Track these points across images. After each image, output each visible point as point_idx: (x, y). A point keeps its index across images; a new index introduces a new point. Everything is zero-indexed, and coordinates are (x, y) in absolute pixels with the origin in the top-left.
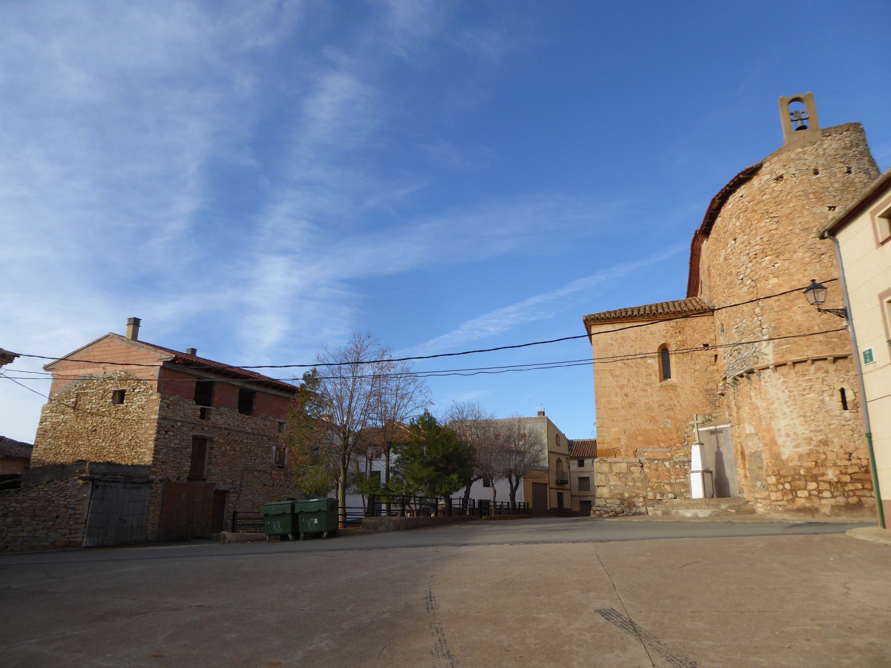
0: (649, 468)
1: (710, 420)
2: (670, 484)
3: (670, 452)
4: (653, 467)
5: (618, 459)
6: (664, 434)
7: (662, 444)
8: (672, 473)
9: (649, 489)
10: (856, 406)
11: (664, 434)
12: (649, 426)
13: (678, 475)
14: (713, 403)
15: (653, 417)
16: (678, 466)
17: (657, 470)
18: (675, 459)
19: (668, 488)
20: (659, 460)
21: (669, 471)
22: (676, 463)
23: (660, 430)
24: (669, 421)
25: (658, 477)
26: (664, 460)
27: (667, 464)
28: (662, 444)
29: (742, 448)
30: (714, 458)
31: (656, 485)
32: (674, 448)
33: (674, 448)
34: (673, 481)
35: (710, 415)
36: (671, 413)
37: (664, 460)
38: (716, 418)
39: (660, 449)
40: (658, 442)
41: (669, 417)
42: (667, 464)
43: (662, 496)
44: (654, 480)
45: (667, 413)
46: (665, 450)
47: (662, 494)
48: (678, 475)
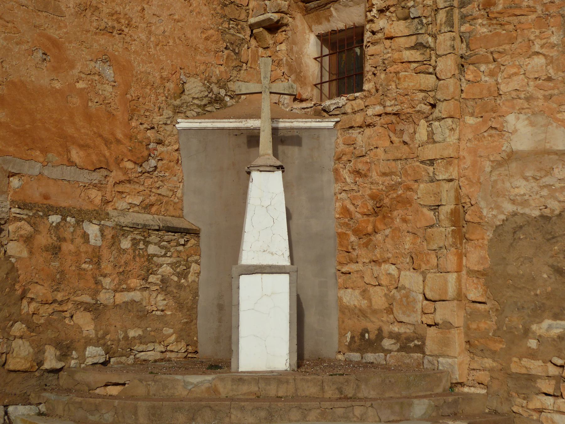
0: (28, 240)
1: (218, 100)
2: (95, 309)
3: (98, 186)
4: (43, 239)
5: (288, 28)
6: (89, 117)
7: (76, 155)
8: (106, 267)
9: (18, 328)
10: (320, 113)
11: (89, 117)
12: (38, 76)
13: (124, 274)
14: (234, 47)
15: (55, 43)
16: (126, 244)
17: (55, 250)
18: (116, 218)
19: (85, 323)
20: (64, 212)
21: (96, 257)
22: (122, 230)
23: (76, 101)
24: (109, 72)
25: (58, 280)
26: (81, 216)
27: (92, 230)
28: (76, 155)
29: (458, 198)
30: (296, 297)
31: (46, 310)
32: (116, 175)
33: (116, 175)
34: (104, 297)
35: (222, 84)
36: (115, 46)
37: (81, 216)
38: (235, 96)
39: (69, 173)
40: (66, 141)
41: (107, 59)
42: (92, 230)
43: (64, 356)
44: (39, 291)
45: (103, 40)
46: (85, 177)
47: (65, 352)
48: (124, 274)
